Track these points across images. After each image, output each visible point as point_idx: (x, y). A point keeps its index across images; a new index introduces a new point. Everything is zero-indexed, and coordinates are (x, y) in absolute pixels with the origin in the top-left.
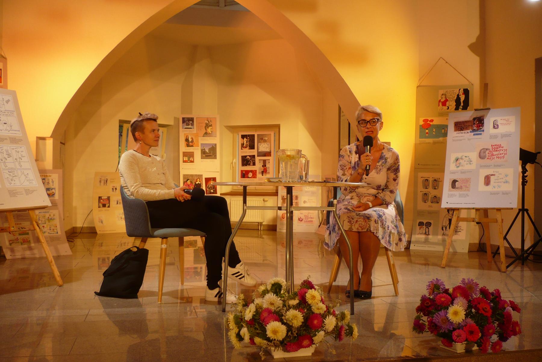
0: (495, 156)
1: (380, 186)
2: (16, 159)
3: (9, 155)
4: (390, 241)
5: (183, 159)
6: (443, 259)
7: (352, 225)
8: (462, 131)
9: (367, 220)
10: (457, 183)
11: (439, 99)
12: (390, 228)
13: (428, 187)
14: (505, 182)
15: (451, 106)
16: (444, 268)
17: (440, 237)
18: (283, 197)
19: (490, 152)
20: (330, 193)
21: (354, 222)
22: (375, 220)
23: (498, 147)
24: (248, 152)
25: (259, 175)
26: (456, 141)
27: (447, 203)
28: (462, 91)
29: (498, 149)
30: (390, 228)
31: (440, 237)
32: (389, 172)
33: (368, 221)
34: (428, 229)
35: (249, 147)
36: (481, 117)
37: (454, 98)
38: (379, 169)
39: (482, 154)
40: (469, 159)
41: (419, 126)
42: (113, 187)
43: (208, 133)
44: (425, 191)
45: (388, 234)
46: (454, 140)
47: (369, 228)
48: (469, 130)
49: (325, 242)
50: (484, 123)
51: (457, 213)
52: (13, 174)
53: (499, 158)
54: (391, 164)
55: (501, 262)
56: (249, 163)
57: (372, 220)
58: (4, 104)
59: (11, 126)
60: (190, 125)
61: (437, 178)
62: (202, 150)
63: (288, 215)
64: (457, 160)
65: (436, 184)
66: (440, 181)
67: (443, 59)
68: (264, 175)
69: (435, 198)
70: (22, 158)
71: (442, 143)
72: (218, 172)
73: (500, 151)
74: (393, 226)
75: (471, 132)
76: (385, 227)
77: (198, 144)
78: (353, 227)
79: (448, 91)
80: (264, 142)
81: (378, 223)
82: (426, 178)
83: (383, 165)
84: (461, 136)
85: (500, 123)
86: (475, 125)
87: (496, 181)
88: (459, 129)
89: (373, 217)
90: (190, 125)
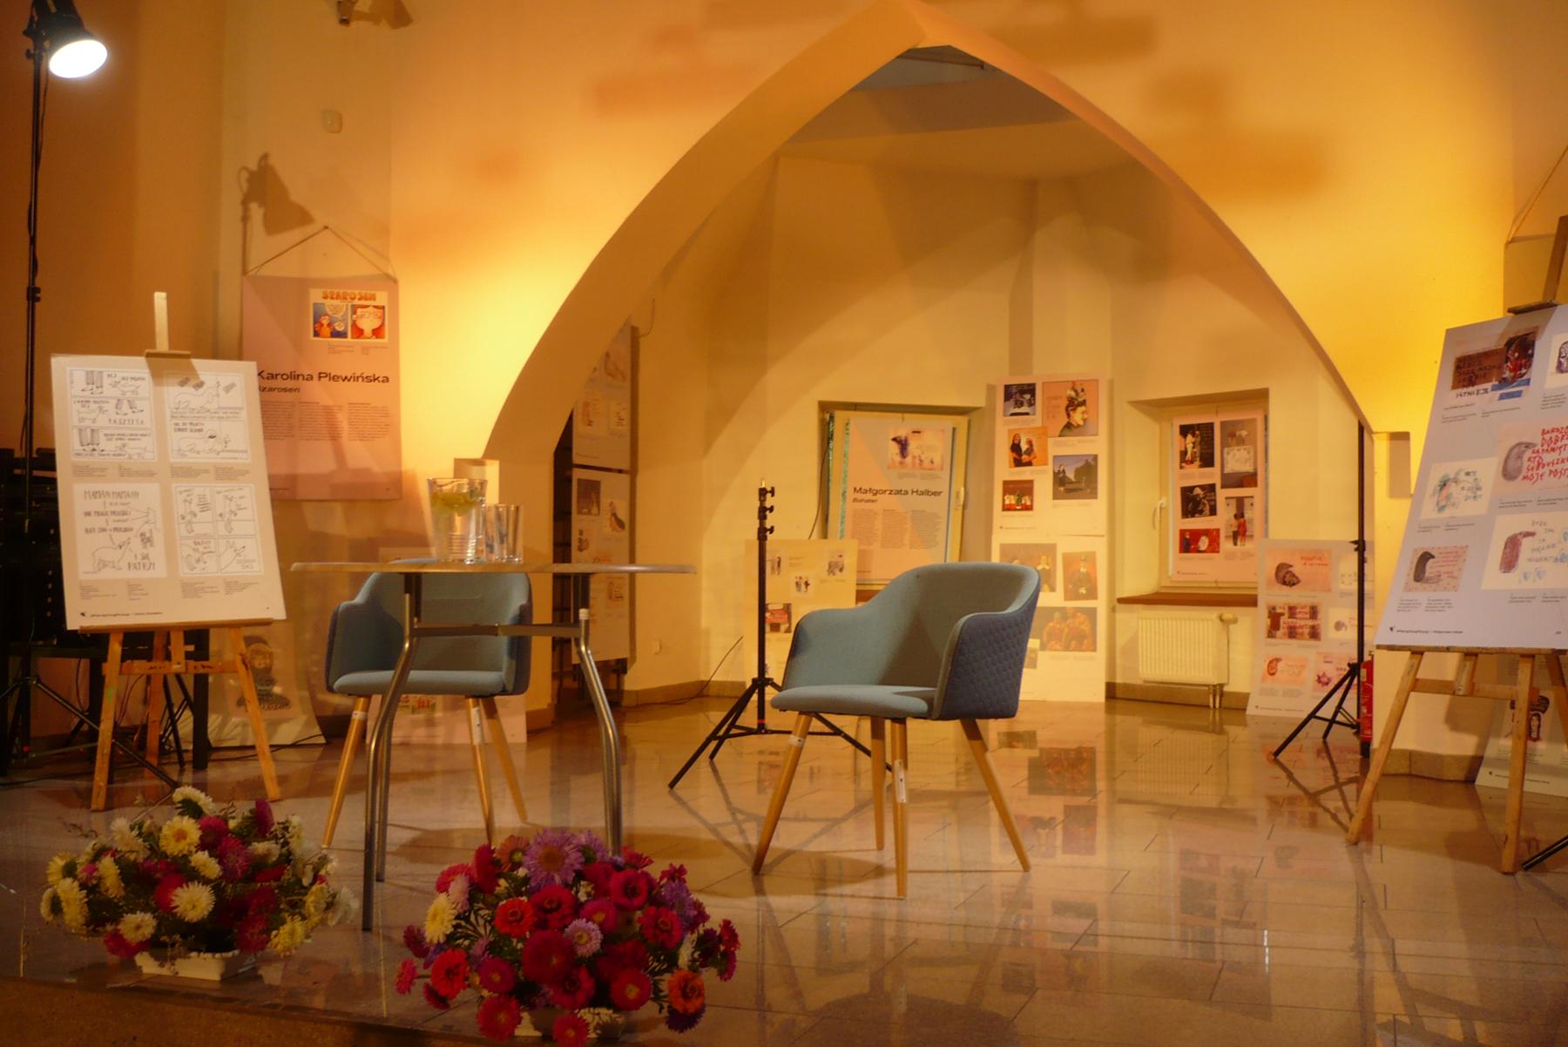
2: (221, 515)
3: (205, 507)
5: (1004, 500)
8: (1473, 385)
10: (1430, 563)
14: (1559, 557)
18: (1274, 608)
19: (1534, 455)
23: (1560, 436)
24: (1198, 476)
25: (1226, 545)
29: (1559, 444)
34: (1539, 720)
35: (1200, 461)
40: (1476, 480)
42: (798, 580)
43: (1073, 426)
48: (1490, 381)
50: (1532, 355)
52: (205, 548)
53: (1555, 476)
56: (1200, 508)
58: (218, 395)
59: (226, 443)
60: (1025, 404)
62: (1056, 475)
64: (1445, 485)
68: (1239, 543)
70: (237, 512)
72: (1103, 536)
77: (1047, 459)
80: (1238, 444)
84: (1468, 405)
88: (1464, 380)
90: (1025, 404)
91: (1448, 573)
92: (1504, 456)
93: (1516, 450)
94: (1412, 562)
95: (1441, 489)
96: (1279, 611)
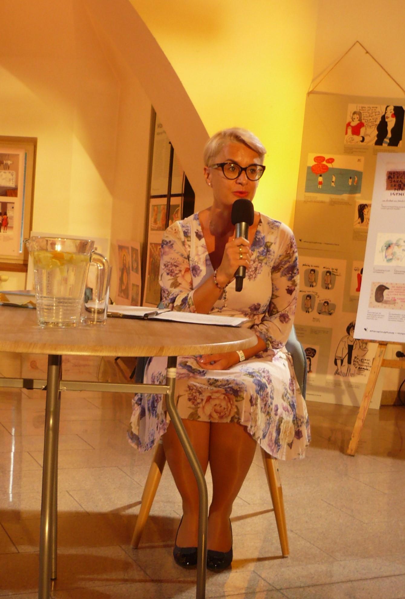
1: (257, 307)
4: (279, 439)
6: (352, 438)
7: (199, 408)
9: (232, 396)
10: (386, 292)
11: (348, 121)
12: (279, 411)
13: (314, 284)
15: (369, 137)
16: (353, 456)
17: (330, 378)
20: (125, 274)
21: (202, 400)
22: (251, 397)
26: (388, 209)
27: (365, 329)
28: (391, 110)
30: (279, 410)
31: (330, 378)
32: (279, 274)
34: (310, 360)
37: (375, 121)
38: (254, 269)
41: (306, 169)
44: (309, 290)
45: (276, 424)
46: (384, 208)
47: (237, 416)
49: (132, 432)
51: (382, 351)
54: (280, 256)
57: (243, 399)
61: (332, 269)
64: (389, 246)
66: (337, 275)
67: (361, 45)
69: (326, 304)
71: (346, 203)
74: (286, 404)
76: (270, 411)
78: (200, 412)
79: (364, 108)
81: (256, 405)
82: (312, 266)
83: (262, 260)
84: (399, 201)
88: (395, 186)
89: (246, 391)
91: (402, 299)
94: (372, 290)
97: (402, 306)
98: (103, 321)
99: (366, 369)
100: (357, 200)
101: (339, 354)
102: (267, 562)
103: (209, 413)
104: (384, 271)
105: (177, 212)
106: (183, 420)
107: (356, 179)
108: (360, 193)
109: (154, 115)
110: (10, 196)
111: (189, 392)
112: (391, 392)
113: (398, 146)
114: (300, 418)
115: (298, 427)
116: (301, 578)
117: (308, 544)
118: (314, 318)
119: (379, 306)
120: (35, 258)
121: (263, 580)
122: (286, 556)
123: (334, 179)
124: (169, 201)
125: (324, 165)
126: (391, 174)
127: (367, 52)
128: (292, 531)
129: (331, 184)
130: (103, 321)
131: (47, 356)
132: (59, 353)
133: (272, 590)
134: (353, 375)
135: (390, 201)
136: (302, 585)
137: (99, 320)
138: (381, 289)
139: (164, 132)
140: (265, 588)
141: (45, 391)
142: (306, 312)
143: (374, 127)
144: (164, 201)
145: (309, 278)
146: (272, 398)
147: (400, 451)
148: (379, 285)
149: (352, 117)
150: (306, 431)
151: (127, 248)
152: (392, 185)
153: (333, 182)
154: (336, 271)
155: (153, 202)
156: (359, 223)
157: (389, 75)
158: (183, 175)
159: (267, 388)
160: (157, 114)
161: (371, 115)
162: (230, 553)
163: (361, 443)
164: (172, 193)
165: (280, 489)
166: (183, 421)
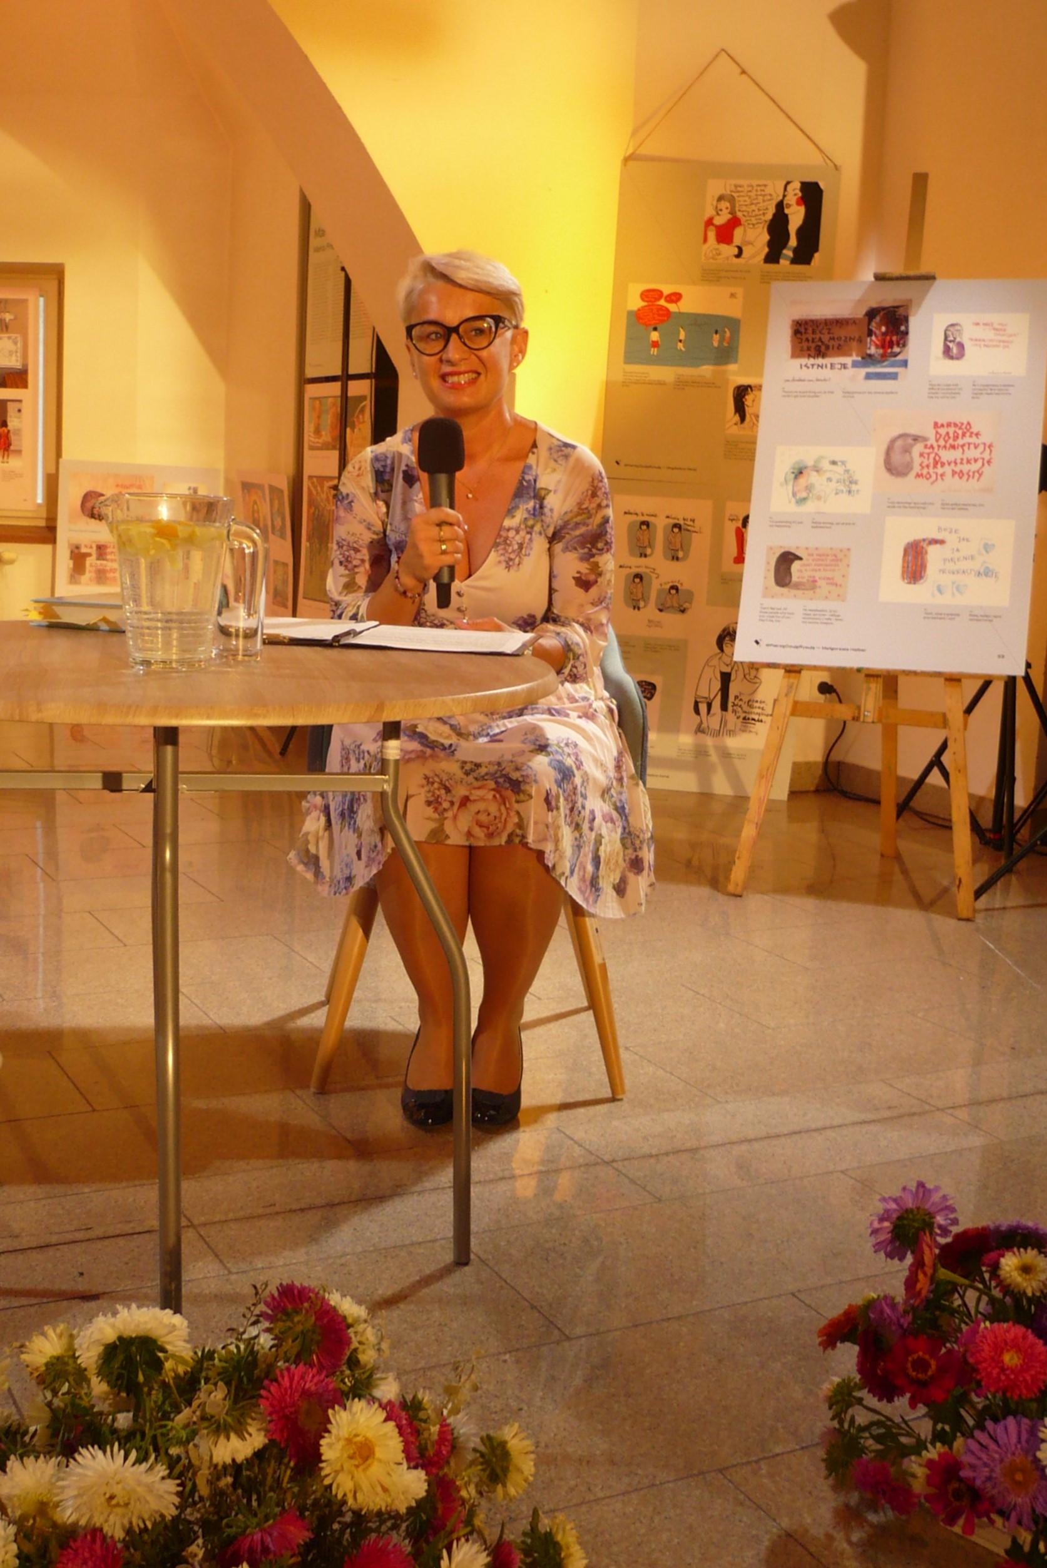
0: (946, 466)
6: (737, 861)
7: (446, 818)
9: (509, 793)
10: (796, 566)
13: (649, 551)
14: (982, 571)
15: (751, 246)
16: (740, 896)
17: (686, 740)
18: (78, 547)
19: (927, 451)
22: (548, 794)
23: (960, 432)
27: (757, 642)
28: (795, 190)
29: (960, 441)
30: (597, 820)
31: (686, 740)
33: (514, 799)
36: (898, 307)
37: (764, 214)
39: (897, 458)
40: (847, 471)
41: (625, 315)
44: (637, 564)
46: (787, 394)
47: (518, 832)
48: (850, 355)
50: (906, 333)
55: (957, 883)
57: (530, 797)
61: (684, 519)
63: (168, 855)
64: (801, 473)
65: (678, 540)
67: (729, 55)
69: (673, 592)
71: (709, 384)
73: (966, 448)
75: (855, 365)
76: (581, 823)
78: (448, 827)
79: (740, 186)
81: (558, 808)
82: (643, 515)
84: (818, 380)
85: (972, 340)
86: (874, 338)
87: (950, 566)
88: (809, 349)
89: (536, 781)
91: (828, 579)
92: (884, 447)
93: (899, 443)
95: (796, 478)
96: (84, 550)
97: (829, 592)
98: (256, 654)
99: (758, 721)
100: (732, 378)
101: (703, 692)
102: (582, 1110)
103: (466, 829)
104: (790, 523)
105: (362, 411)
106: (418, 843)
107: (728, 334)
108: (736, 362)
109: (306, 208)
110: (12, 387)
111: (426, 788)
112: (808, 765)
113: (812, 264)
114: (638, 833)
115: (635, 850)
116: (650, 1138)
117: (660, 1072)
118: (649, 621)
119: (782, 595)
120: (120, 536)
121: (576, 1146)
122: (619, 1097)
123: (682, 336)
124: (345, 389)
125: (662, 308)
126: (800, 325)
127: (743, 72)
128: (627, 1049)
129: (677, 345)
130: (256, 654)
131: (152, 731)
132: (173, 722)
133: (596, 1164)
134: (731, 733)
135: (800, 380)
136: (654, 1153)
137: (248, 653)
138: (786, 559)
139: (330, 246)
140: (581, 1161)
141: (150, 796)
142: (634, 608)
143: (761, 226)
144: (335, 388)
145: (638, 540)
146: (584, 797)
147: (831, 882)
148: (782, 551)
149: (717, 207)
150: (648, 856)
151: (260, 487)
152: (802, 347)
153: (680, 341)
154: (691, 523)
155: (312, 390)
156: (736, 424)
157: (789, 117)
158: (371, 334)
159: (574, 776)
160: (313, 208)
161: (755, 202)
162: (517, 1094)
163: (753, 870)
164: (351, 371)
165: (603, 967)
166: (417, 845)
